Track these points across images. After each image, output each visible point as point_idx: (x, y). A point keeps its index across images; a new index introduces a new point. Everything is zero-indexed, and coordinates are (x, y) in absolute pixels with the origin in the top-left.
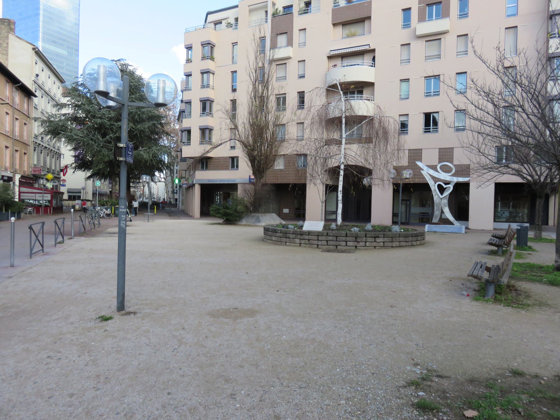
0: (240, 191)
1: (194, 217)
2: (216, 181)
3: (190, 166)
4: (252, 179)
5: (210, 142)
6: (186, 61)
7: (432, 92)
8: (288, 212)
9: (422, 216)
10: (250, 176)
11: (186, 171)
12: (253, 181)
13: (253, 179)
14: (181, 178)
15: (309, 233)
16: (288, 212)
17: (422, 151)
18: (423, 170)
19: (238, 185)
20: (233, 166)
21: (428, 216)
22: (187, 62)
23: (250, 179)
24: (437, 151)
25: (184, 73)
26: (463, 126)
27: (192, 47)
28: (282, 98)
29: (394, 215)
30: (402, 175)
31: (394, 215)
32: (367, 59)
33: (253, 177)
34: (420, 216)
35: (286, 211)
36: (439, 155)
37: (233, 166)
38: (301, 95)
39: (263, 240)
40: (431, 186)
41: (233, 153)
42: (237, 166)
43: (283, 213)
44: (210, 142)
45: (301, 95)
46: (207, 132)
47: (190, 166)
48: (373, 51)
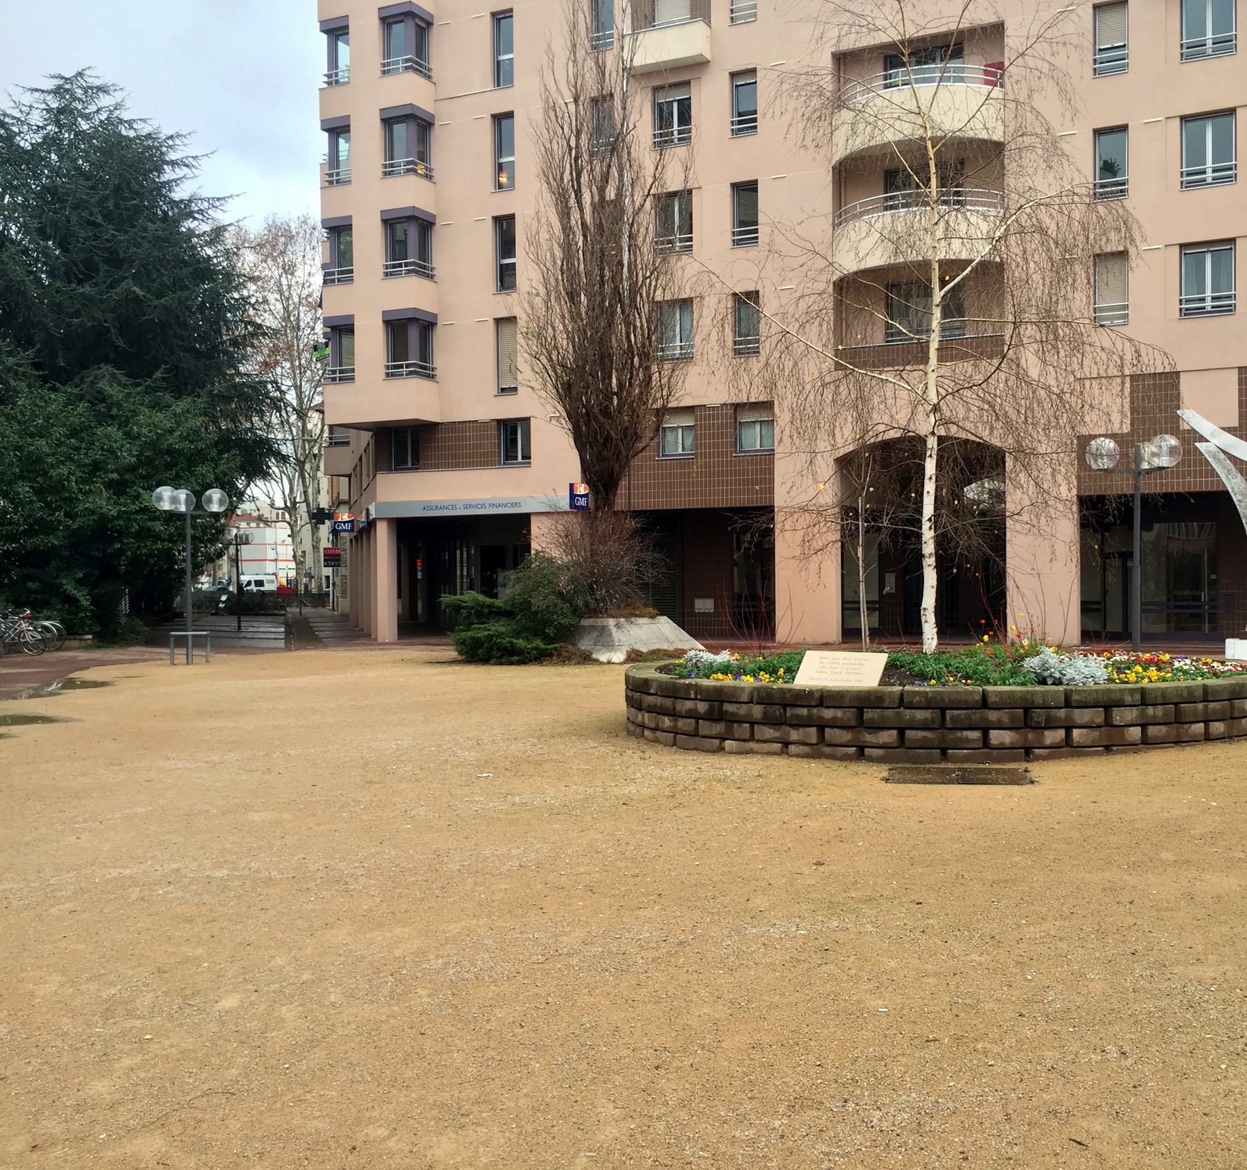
0: (542, 538)
1: (376, 639)
2: (454, 507)
3: (361, 459)
4: (581, 496)
5: (425, 368)
6: (326, 79)
7: (1209, 170)
8: (1228, 641)
9: (1176, 607)
10: (572, 486)
11: (349, 476)
12: (582, 502)
13: (586, 496)
14: (338, 506)
15: (824, 698)
16: (1228, 641)
17: (1178, 378)
18: (1202, 439)
19: (533, 519)
20: (507, 458)
21: (1200, 607)
22: (329, 83)
23: (573, 496)
24: (1235, 375)
25: (323, 121)
26: (1123, 383)
27: (347, 27)
28: (675, 105)
29: (846, 606)
30: (1138, 459)
31: (846, 606)
32: (973, 65)
33: (582, 489)
34: (1168, 607)
35: (704, 605)
36: (1240, 390)
37: (510, 456)
38: (745, 192)
39: (609, 731)
40: (1235, 499)
41: (509, 409)
42: (527, 456)
43: (693, 613)
44: (425, 368)
45: (745, 192)
46: (413, 334)
47: (361, 459)
48: (995, 32)
